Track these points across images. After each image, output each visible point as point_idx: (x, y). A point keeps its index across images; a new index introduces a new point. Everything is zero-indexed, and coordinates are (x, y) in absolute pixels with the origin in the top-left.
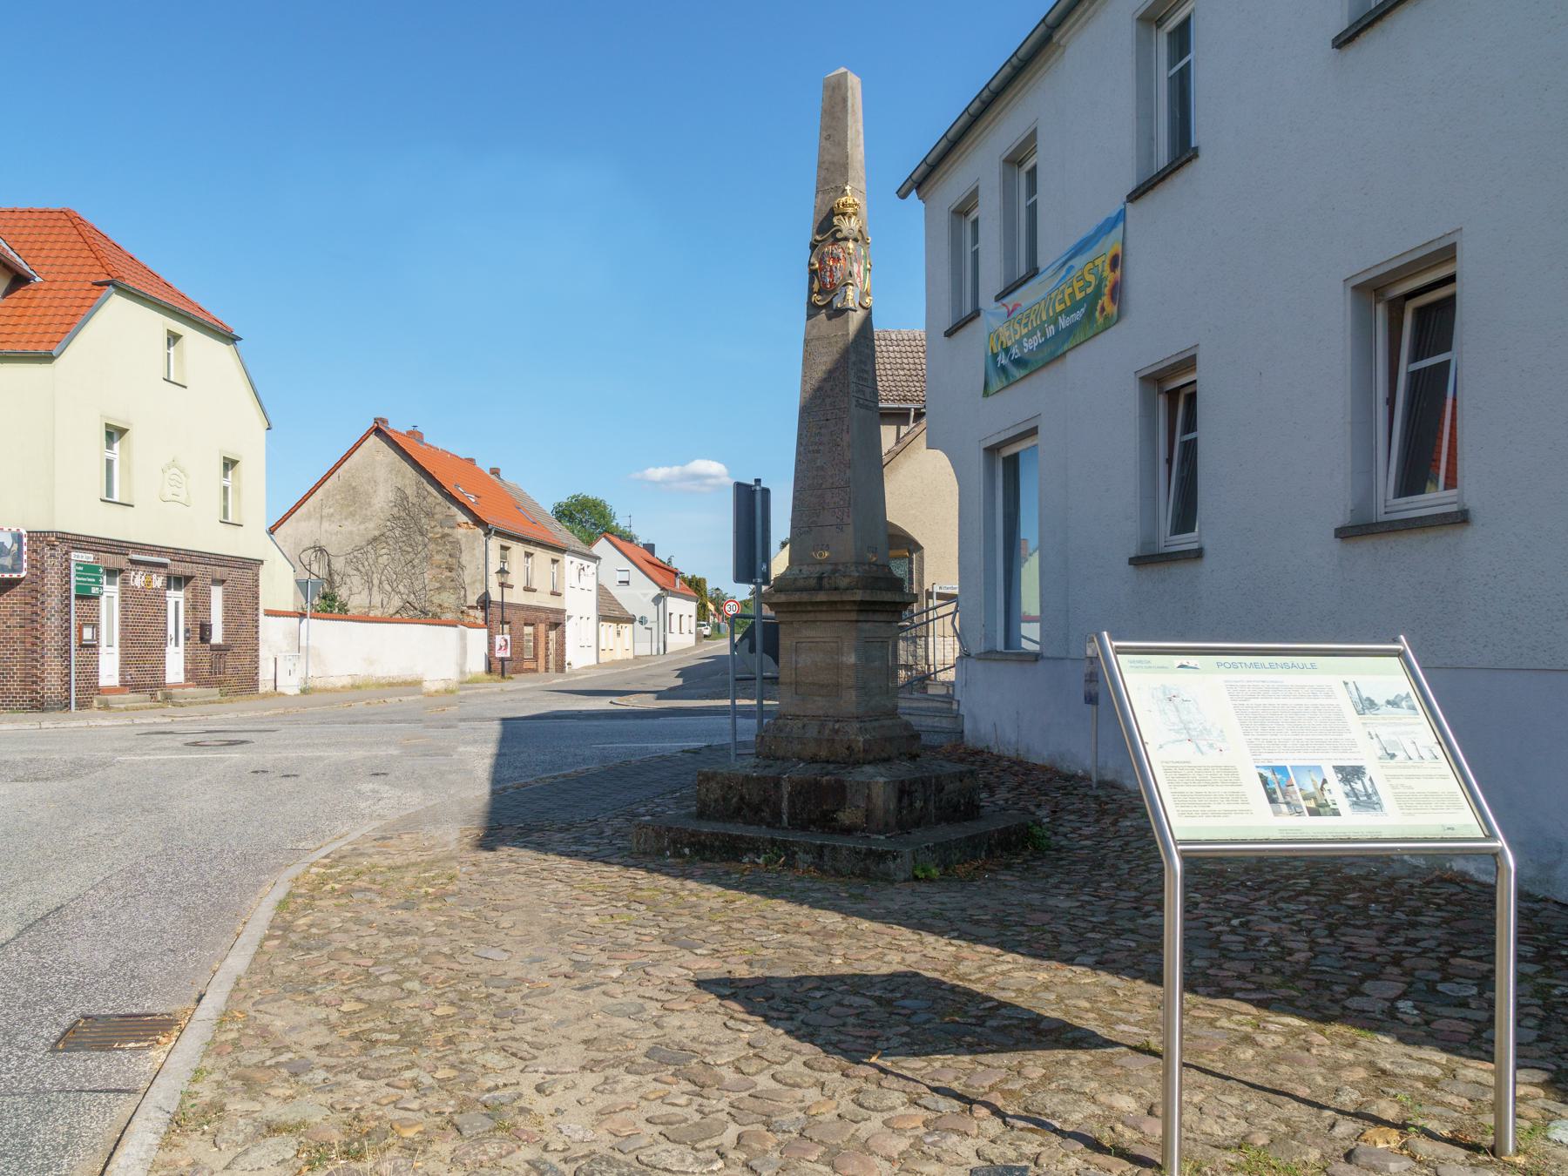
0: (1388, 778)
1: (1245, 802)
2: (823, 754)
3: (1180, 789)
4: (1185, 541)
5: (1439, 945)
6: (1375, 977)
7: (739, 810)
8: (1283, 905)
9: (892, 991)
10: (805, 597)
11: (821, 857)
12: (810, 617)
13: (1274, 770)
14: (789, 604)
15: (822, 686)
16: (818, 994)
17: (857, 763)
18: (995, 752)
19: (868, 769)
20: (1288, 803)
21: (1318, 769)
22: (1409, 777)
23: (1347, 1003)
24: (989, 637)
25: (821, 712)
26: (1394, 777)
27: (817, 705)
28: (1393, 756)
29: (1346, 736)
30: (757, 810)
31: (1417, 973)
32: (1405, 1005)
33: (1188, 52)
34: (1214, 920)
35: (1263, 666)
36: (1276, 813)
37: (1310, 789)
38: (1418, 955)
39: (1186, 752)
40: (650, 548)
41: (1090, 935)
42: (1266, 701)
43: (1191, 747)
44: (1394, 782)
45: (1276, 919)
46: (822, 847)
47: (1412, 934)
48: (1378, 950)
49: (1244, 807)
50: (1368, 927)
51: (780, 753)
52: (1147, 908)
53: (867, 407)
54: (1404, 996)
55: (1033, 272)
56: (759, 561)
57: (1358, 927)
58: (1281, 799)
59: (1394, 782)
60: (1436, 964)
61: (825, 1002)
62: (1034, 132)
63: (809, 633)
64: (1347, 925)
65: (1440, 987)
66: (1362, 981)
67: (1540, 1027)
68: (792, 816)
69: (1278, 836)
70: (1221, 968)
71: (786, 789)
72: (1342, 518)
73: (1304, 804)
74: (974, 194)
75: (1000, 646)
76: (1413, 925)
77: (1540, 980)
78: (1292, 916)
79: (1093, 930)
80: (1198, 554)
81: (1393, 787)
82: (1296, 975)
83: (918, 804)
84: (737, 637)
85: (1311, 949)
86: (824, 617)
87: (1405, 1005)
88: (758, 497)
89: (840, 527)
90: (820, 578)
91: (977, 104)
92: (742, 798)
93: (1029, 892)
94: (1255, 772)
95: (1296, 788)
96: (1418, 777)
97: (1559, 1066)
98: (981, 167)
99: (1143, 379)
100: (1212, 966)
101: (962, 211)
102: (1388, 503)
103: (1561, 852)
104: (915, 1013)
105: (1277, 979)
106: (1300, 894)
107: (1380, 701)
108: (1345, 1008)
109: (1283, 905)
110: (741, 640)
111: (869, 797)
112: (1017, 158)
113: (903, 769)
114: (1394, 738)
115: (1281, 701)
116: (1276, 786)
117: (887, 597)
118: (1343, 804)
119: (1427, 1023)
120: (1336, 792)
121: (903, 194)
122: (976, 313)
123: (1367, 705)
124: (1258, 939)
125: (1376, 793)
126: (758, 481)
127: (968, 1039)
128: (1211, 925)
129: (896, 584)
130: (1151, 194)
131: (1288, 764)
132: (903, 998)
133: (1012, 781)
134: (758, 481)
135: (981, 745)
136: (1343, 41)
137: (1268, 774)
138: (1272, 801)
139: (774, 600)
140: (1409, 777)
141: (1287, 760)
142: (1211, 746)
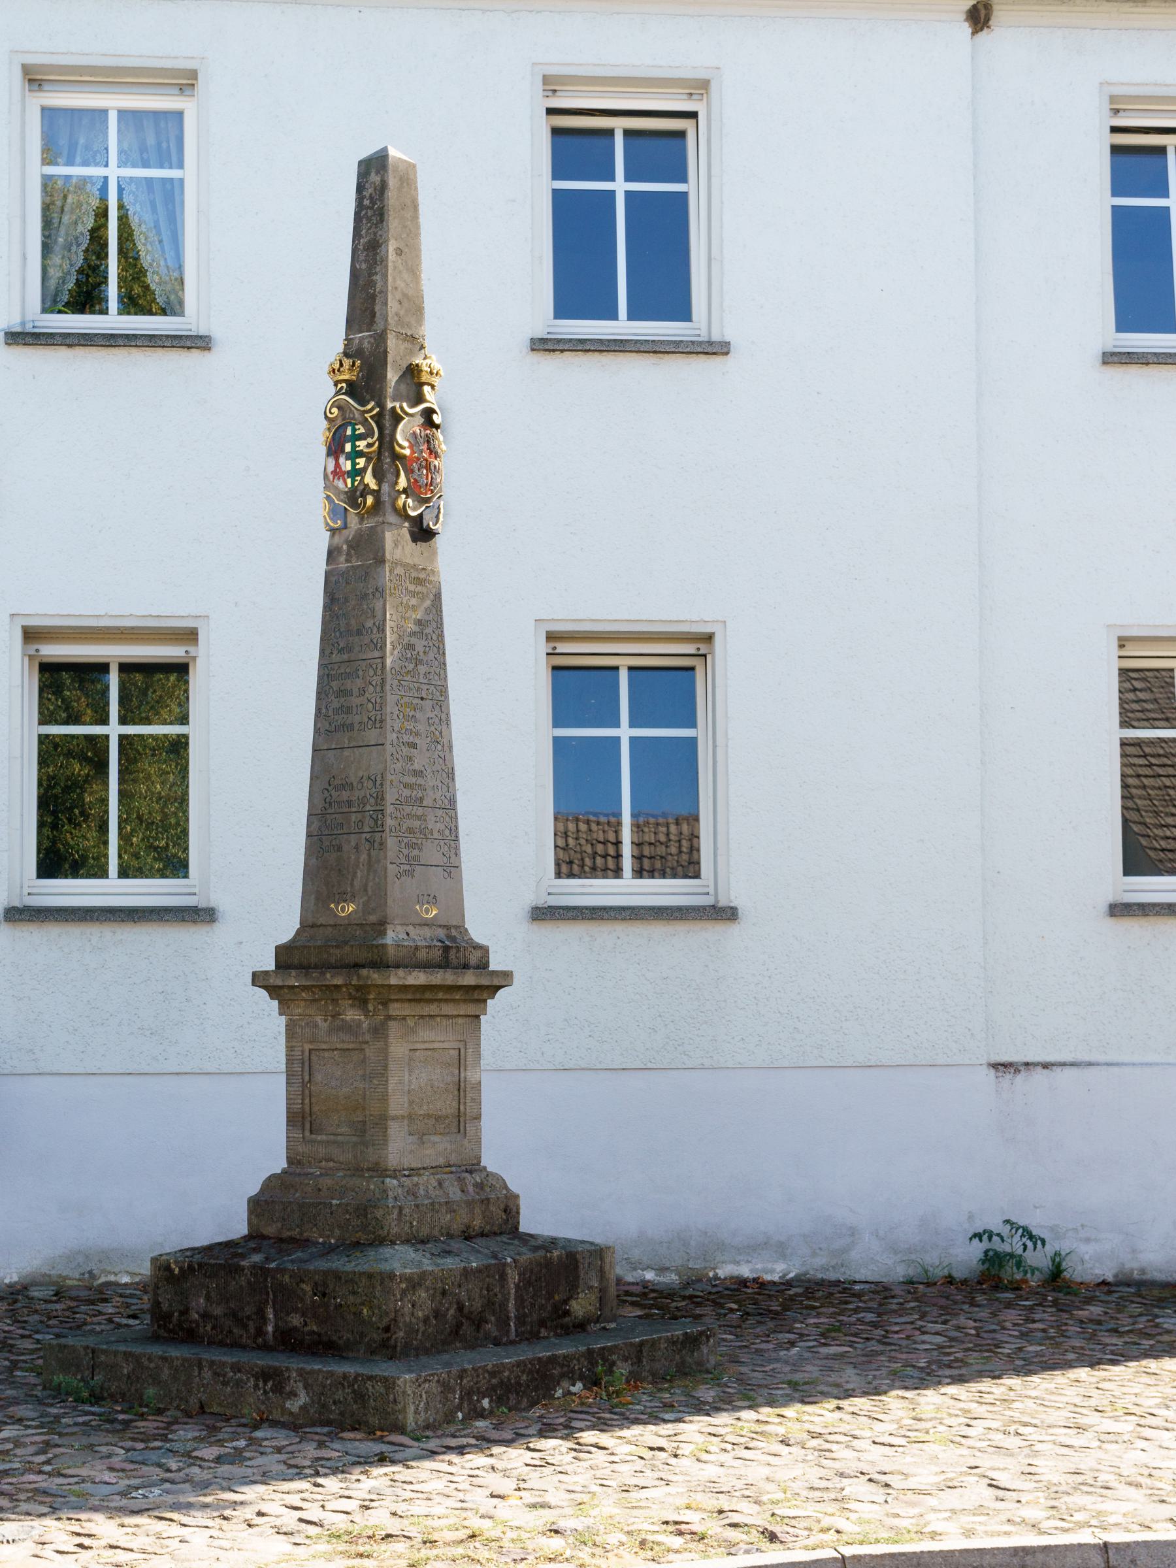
7: (456, 1331)
30: (478, 1322)
51: (425, 1231)
68: (521, 1320)
71: (513, 1277)
92: (460, 1308)
103: (853, 1235)
111: (601, 1271)
117: (469, 979)
139: (273, 981)
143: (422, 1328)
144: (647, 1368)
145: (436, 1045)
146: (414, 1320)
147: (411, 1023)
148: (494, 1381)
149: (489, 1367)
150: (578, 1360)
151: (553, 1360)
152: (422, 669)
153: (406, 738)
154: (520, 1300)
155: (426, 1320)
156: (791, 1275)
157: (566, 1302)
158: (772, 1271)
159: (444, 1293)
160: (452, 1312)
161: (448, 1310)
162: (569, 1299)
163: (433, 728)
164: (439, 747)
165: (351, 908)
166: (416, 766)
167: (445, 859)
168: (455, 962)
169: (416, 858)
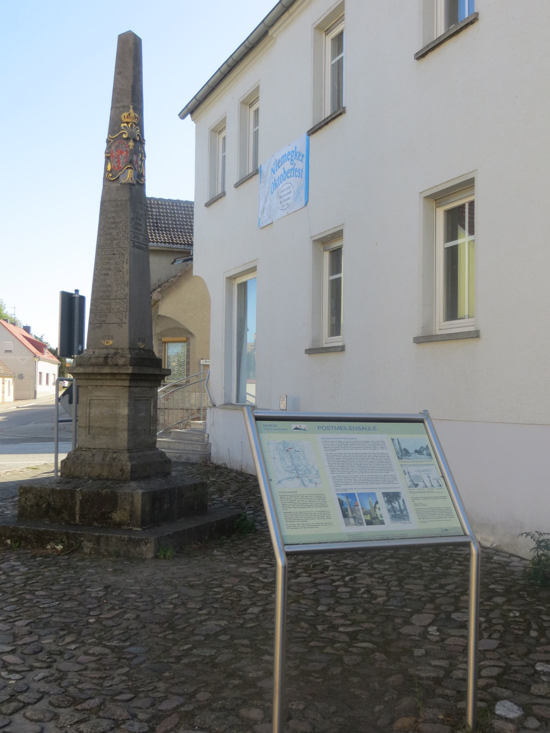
0: (413, 499)
1: (329, 518)
2: (105, 474)
3: (289, 510)
4: (336, 341)
5: (457, 588)
6: (418, 611)
8: (376, 566)
9: (124, 641)
10: (96, 370)
11: (98, 543)
12: (99, 383)
13: (348, 496)
14: (85, 374)
15: (106, 429)
16: (73, 647)
17: (125, 481)
18: (229, 467)
19: (133, 484)
20: (354, 518)
21: (373, 494)
22: (425, 498)
23: (401, 631)
24: (227, 395)
25: (105, 446)
26: (417, 498)
27: (102, 442)
28: (416, 485)
29: (391, 473)
31: (442, 607)
32: (432, 630)
33: (342, 51)
34: (336, 578)
35: (345, 428)
36: (347, 524)
37: (368, 508)
38: (445, 595)
39: (293, 485)
40: (27, 329)
41: (260, 592)
42: (346, 451)
43: (297, 482)
44: (416, 502)
45: (371, 576)
46: (99, 537)
47: (443, 582)
48: (423, 593)
49: (327, 521)
50: (421, 578)
51: (77, 473)
52: (298, 571)
53: (140, 248)
54: (432, 624)
55: (256, 172)
56: (76, 344)
57: (416, 578)
58: (350, 514)
59: (416, 502)
60: (452, 600)
61: (76, 653)
62: (258, 87)
63: (98, 393)
64: (409, 577)
65: (454, 616)
66: (412, 614)
67: (501, 638)
68: (82, 516)
69: (347, 539)
70: (334, 611)
71: (79, 498)
72: (417, 332)
73: (363, 518)
74: (224, 120)
75: (234, 401)
76: (445, 575)
77: (504, 608)
78: (380, 572)
79: (263, 588)
80: (342, 349)
81: (415, 505)
82: (376, 613)
83: (166, 506)
84: (61, 393)
85: (387, 595)
86: (108, 383)
87: (432, 630)
88: (77, 302)
89: (120, 324)
90: (106, 358)
91: (225, 67)
92: (49, 504)
93: (230, 563)
94: (336, 497)
95: (360, 507)
96: (430, 498)
97: (507, 663)
98: (227, 103)
99: (315, 241)
100: (328, 610)
101: (218, 129)
102: (443, 326)
104: (136, 656)
105: (364, 617)
106: (387, 558)
107: (411, 451)
108: (400, 634)
109: (376, 566)
110: (64, 395)
112: (250, 101)
113: (157, 484)
114: (418, 474)
115: (354, 451)
116: (348, 507)
118: (386, 516)
119: (443, 640)
120: (383, 510)
121: (182, 116)
122: (223, 194)
123: (403, 453)
124: (359, 589)
125: (406, 509)
126: (77, 291)
127: (167, 674)
128: (334, 581)
129: (157, 363)
130: (320, 132)
131: (356, 492)
132: (131, 645)
133: (234, 486)
134: (77, 291)
135: (220, 463)
136: (421, 56)
137: (344, 499)
138: (345, 516)
139: (76, 371)
140: (425, 498)
141: (355, 489)
142: (311, 481)
143: (29, 509)
144: (104, 548)
145: (103, 398)
146: (26, 505)
147: (90, 388)
148: (13, 534)
149: (11, 527)
150: (60, 535)
151: (46, 532)
152: (115, 242)
153: (103, 272)
154: (82, 506)
155: (31, 506)
156: (495, 545)
157: (110, 513)
158: (487, 540)
159: (41, 497)
160: (44, 505)
161: (43, 504)
162: (111, 512)
163: (118, 266)
164: (121, 273)
165: (111, 342)
166: (108, 283)
167: (119, 320)
168: (111, 363)
169: (104, 321)
